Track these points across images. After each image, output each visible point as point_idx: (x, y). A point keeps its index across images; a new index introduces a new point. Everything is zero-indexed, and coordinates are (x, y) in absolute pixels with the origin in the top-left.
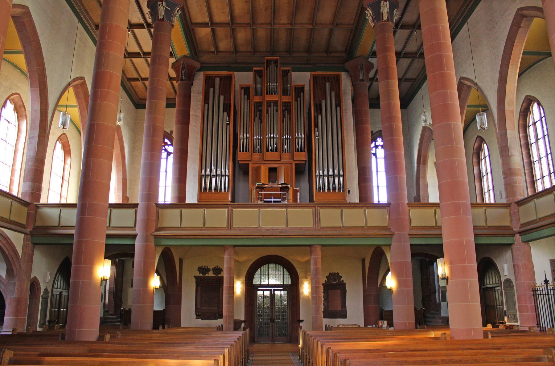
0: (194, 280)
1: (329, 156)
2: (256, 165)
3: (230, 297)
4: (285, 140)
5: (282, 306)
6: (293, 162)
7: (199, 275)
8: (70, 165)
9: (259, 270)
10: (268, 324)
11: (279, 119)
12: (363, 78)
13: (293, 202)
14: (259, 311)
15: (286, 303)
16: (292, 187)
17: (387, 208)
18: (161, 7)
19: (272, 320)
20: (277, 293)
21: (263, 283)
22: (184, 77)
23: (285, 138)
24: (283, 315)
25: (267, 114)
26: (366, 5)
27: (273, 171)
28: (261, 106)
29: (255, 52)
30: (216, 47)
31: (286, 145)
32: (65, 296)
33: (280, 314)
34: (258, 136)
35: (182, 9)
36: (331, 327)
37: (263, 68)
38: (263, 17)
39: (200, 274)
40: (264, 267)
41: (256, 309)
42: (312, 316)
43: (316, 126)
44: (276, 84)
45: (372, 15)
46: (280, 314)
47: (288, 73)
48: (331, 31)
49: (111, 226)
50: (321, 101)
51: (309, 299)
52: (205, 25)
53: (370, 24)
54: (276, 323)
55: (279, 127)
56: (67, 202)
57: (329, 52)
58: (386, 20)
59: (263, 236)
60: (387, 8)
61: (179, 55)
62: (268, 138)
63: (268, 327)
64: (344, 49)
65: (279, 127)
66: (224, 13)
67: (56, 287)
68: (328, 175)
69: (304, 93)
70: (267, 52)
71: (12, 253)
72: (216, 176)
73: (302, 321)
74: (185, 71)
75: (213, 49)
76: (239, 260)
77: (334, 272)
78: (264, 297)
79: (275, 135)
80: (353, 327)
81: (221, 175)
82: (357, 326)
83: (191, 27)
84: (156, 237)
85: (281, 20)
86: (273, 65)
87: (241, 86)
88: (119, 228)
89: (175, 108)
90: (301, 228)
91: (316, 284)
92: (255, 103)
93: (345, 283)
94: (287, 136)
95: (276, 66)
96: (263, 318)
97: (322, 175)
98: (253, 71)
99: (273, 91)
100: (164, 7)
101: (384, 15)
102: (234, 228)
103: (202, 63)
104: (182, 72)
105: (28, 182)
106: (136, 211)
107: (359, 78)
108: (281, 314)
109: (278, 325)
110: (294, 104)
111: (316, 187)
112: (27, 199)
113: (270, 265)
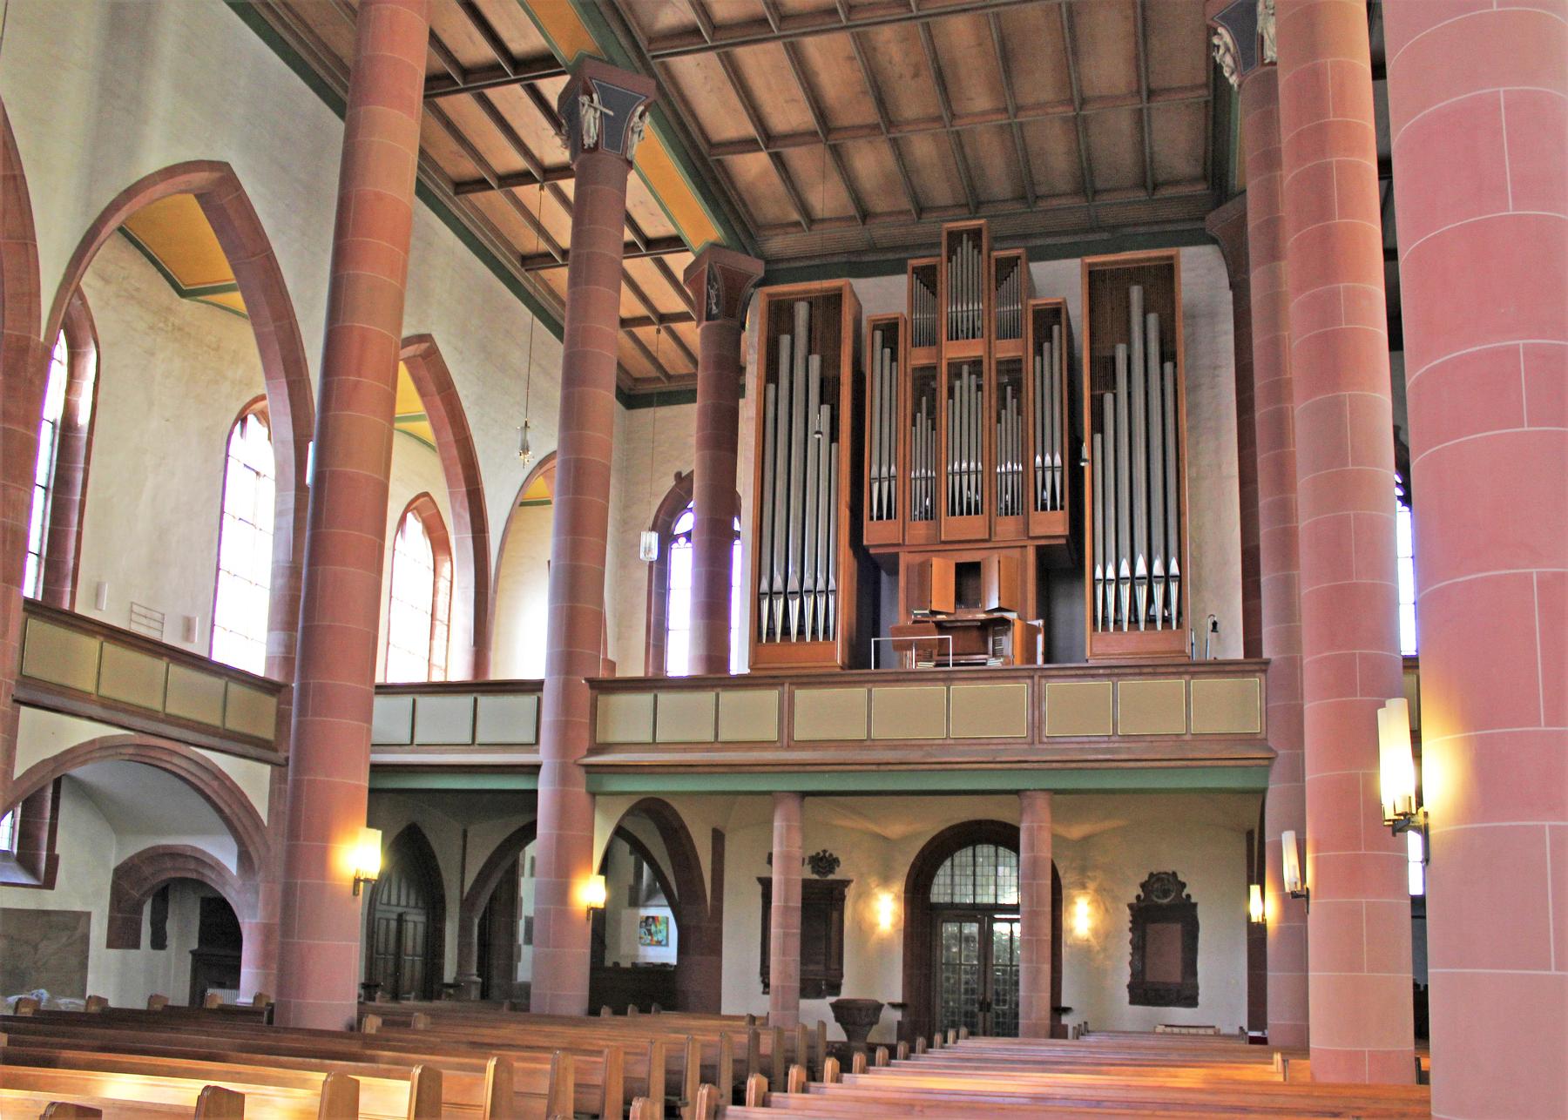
1: (1136, 517)
2: (918, 558)
4: (1004, 477)
6: (1029, 542)
8: (449, 579)
9: (948, 863)
13: (1022, 663)
14: (948, 979)
17: (1258, 674)
21: (1001, 901)
22: (714, 307)
23: (1003, 469)
25: (951, 401)
26: (1212, 19)
27: (968, 573)
28: (934, 378)
30: (805, 209)
32: (415, 926)
34: (923, 471)
37: (938, 259)
38: (914, 100)
43: (1098, 426)
45: (1232, 49)
48: (1140, 120)
49: (477, 742)
50: (1114, 347)
51: (1089, 947)
52: (747, 145)
56: (448, 680)
59: (879, 764)
62: (1043, 468)
64: (1199, 171)
67: (385, 900)
70: (957, 206)
71: (242, 813)
72: (801, 594)
73: (1067, 1010)
74: (718, 290)
75: (795, 216)
77: (1162, 870)
79: (973, 465)
80: (1197, 1035)
81: (815, 592)
82: (1210, 1031)
84: (589, 769)
85: (972, 99)
86: (966, 246)
88: (495, 747)
89: (695, 401)
94: (1009, 466)
95: (977, 246)
98: (910, 269)
100: (595, 109)
103: (767, 262)
104: (708, 292)
105: (277, 629)
106: (539, 700)
109: (1001, 1020)
110: (1030, 364)
112: (276, 677)
113: (979, 848)
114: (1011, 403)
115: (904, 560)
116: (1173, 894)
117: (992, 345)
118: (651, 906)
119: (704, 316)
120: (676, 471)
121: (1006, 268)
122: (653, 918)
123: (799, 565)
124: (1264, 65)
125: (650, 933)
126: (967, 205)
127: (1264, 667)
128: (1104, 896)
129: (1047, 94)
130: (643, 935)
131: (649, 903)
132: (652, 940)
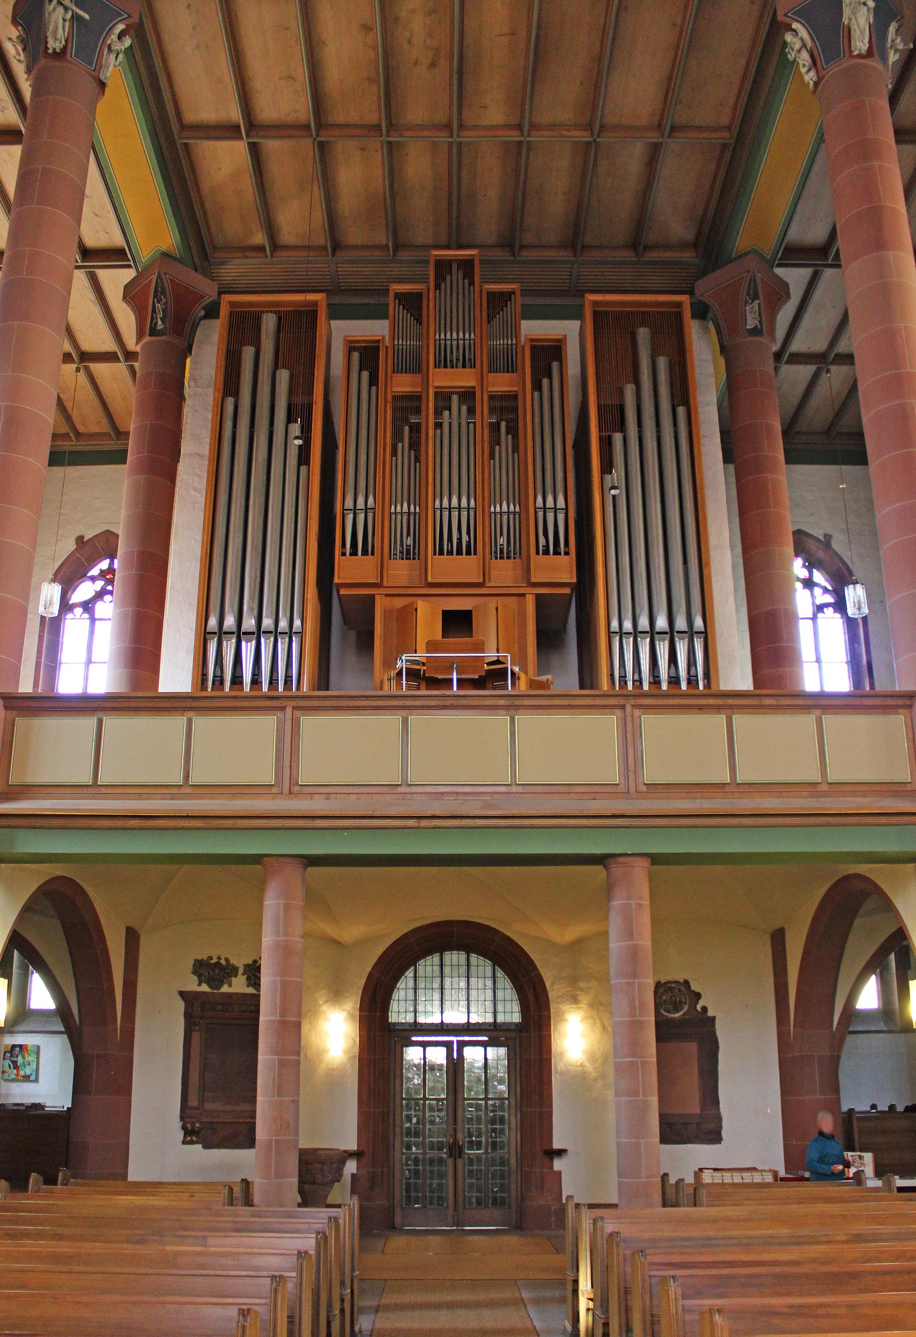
0: (181, 1005)
2: (399, 603)
3: (282, 1064)
4: (499, 516)
5: (490, 1099)
7: (200, 989)
9: (410, 973)
10: (441, 1161)
11: (479, 450)
12: (756, 326)
14: (409, 1118)
15: (503, 1088)
16: (526, 674)
17: (901, 711)
18: (54, 10)
19: (455, 1150)
20: (473, 1055)
21: (422, 1019)
22: (160, 322)
23: (498, 509)
24: (494, 1130)
25: (439, 431)
26: (785, 15)
28: (418, 411)
29: (397, 248)
31: (501, 534)
33: (482, 1126)
34: (405, 505)
35: (137, 30)
36: (677, 1183)
39: (199, 985)
40: (428, 962)
41: (398, 1112)
42: (618, 1144)
44: (467, 336)
46: (482, 1126)
47: (509, 302)
48: (654, 153)
51: (584, 1073)
52: (228, 131)
53: (801, 76)
54: (469, 1158)
55: (479, 472)
57: (641, 248)
58: (864, 51)
59: (420, 818)
60: (868, 9)
61: (145, 252)
63: (442, 1175)
64: (690, 236)
65: (479, 472)
66: (289, 77)
68: (652, 633)
69: (563, 361)
72: (258, 633)
73: (561, 1153)
74: (165, 304)
75: (259, 238)
76: (338, 938)
78: (426, 1068)
83: (180, 138)
87: (351, 342)
90: (568, 789)
91: (632, 1014)
92: (397, 398)
93: (714, 1018)
96: (423, 1143)
97: (632, 631)
99: (458, 359)
101: (856, 34)
102: (306, 790)
107: (746, 325)
108: (486, 1127)
111: (612, 675)
113: (447, 956)
114: (506, 439)
115: (380, 605)
116: (686, 1008)
117: (485, 378)
118: (19, 1032)
119: (148, 332)
120: (77, 534)
121: (498, 302)
122: (21, 1046)
123: (256, 600)
124: (851, 56)
125: (16, 1067)
126: (387, 246)
127: (908, 702)
128: (599, 1008)
129: (565, 115)
130: (7, 1069)
131: (17, 1029)
132: (17, 1075)
